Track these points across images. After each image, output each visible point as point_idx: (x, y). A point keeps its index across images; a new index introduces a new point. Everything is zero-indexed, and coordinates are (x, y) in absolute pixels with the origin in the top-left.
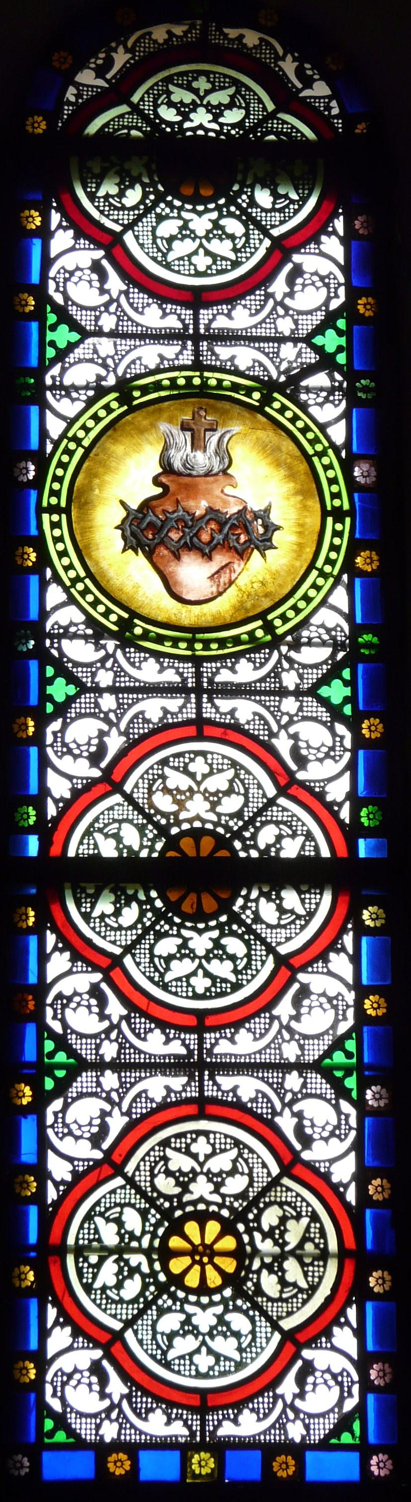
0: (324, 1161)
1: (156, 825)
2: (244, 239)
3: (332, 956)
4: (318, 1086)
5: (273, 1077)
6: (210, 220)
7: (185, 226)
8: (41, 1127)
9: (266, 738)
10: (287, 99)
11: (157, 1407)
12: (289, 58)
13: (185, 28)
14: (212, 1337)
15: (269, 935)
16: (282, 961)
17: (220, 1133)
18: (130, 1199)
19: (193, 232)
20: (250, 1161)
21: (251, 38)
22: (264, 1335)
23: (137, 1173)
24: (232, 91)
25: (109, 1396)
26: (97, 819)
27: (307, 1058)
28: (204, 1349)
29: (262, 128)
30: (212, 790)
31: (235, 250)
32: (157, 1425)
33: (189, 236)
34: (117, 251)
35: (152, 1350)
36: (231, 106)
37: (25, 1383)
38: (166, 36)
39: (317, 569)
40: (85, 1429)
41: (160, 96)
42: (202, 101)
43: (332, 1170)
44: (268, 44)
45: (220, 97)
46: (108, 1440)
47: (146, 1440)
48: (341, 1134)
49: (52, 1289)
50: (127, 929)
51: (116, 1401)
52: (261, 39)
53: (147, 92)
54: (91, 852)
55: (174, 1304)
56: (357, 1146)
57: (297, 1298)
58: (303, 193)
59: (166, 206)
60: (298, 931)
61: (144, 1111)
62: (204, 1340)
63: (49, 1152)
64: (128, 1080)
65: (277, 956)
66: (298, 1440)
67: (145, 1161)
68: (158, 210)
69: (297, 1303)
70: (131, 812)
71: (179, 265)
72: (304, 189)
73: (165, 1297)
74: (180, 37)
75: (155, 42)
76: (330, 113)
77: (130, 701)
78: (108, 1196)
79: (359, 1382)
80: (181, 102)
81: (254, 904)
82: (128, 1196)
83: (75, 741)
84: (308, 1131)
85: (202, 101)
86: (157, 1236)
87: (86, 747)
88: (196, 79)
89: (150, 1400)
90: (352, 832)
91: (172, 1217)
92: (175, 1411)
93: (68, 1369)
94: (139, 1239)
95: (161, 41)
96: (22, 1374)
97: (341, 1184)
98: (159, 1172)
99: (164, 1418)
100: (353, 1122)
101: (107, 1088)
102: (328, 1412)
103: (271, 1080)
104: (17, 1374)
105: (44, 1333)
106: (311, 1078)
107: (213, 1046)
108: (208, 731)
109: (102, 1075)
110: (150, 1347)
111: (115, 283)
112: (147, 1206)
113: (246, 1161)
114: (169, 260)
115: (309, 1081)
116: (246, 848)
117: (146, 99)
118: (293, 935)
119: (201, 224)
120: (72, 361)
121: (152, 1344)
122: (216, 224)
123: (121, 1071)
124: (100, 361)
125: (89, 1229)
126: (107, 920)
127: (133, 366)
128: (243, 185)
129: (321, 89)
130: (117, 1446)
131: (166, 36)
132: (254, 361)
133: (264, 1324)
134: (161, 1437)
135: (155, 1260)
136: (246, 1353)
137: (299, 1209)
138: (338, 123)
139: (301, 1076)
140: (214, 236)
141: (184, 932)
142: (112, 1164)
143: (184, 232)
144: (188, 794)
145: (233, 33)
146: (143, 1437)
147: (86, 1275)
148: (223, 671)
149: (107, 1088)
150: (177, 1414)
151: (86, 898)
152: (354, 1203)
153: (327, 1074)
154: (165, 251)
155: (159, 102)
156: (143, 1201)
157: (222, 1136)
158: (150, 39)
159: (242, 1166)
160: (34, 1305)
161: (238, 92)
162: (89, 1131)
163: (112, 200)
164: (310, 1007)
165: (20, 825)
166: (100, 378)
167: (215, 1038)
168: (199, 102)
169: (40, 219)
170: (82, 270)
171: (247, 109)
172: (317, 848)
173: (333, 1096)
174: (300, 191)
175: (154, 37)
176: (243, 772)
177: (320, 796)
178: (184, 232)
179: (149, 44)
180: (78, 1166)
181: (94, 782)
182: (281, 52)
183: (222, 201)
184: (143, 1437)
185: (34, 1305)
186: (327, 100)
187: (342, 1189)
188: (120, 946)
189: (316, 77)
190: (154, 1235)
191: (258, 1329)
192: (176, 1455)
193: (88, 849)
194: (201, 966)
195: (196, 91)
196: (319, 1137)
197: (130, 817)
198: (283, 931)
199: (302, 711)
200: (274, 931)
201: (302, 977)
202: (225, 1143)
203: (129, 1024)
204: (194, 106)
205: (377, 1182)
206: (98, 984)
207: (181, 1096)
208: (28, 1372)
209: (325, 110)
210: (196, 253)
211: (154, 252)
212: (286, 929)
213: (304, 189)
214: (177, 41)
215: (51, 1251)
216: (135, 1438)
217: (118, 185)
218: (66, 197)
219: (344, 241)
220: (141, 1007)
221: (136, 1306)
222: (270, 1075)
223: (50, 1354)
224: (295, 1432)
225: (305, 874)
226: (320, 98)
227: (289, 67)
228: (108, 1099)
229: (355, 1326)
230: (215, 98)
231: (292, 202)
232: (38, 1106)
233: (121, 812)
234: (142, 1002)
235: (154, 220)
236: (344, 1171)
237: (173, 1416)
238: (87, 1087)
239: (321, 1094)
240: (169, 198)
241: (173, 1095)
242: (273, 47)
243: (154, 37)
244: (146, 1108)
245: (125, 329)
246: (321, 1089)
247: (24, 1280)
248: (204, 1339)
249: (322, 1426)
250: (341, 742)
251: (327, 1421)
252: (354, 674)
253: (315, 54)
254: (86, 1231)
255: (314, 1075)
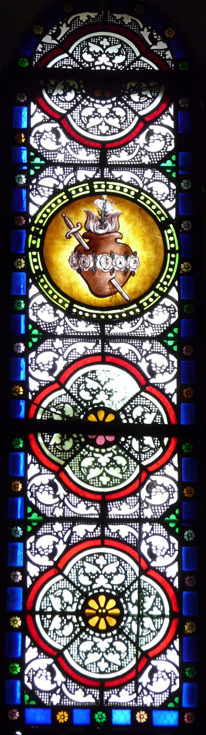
0: (162, 384)
1: (81, 591)
2: (125, 118)
3: (168, 651)
4: (159, 348)
5: (137, 343)
6: (108, 108)
7: (96, 111)
8: (25, 550)
9: (135, 362)
10: (146, 51)
11: (80, 688)
12: (146, 29)
13: (96, 14)
14: (107, 653)
15: (134, 107)
16: (143, 469)
17: (110, 554)
18: (68, 400)
19: (99, 114)
20: (125, 567)
21: (127, 20)
22: (133, 466)
23: (70, 574)
24: (119, 46)
25: (56, 682)
26: (50, 588)
27: (156, 704)
28: (103, 660)
29: (133, 65)
30: (108, 572)
31: (120, 123)
32: (79, 697)
33: (97, 116)
34: (60, 660)
35: (79, 475)
36: (119, 54)
37: (16, 627)
38: (87, 18)
39: (160, 283)
40: (44, 699)
41: (84, 48)
42: (104, 51)
43: (165, 387)
44: (136, 22)
45: (113, 50)
46: (55, 704)
47: (74, 704)
48: (169, 371)
49: (28, 629)
50: (69, 102)
51: (59, 685)
52: (132, 20)
53: (78, 46)
54: (49, 417)
55: (89, 453)
56: (179, 559)
57: (150, 452)
58: (154, 95)
59: (86, 634)
60: (148, 105)
61: (75, 542)
62: (102, 388)
63: (30, 378)
64: (68, 171)
65: (139, 116)
66: (149, 705)
67: (73, 568)
68: (82, 453)
69: (149, 454)
70: (70, 399)
71: (92, 130)
72: (154, 93)
73: (84, 633)
74: (94, 18)
75: (81, 21)
76: (165, 57)
77: (70, 171)
78: (58, 398)
79: (179, 677)
80: (94, 52)
81: (130, 441)
82: (69, 62)
83: (41, 363)
84: (154, 369)
85: (104, 51)
86: (80, 604)
87: (45, 489)
88: (102, 40)
89: (76, 684)
90: (177, 408)
91: (87, 595)
92: (88, 690)
93: (38, 484)
94: (71, 606)
95: (84, 21)
96: (18, 306)
97: (169, 394)
98: (85, 52)
99: (83, 693)
100: (176, 547)
101: (56, 530)
102: (164, 692)
103: (136, 345)
104: (15, 349)
105: (27, 467)
106: (155, 344)
107: (108, 698)
108: (107, 542)
109: (55, 341)
110: (78, 474)
111: (60, 678)
112: (79, 66)
113: (123, 567)
114: (88, 127)
115: (154, 345)
116: (127, 418)
117: (77, 50)
118: (146, 107)
119: (104, 110)
120: (42, 176)
121: (79, 473)
122: (111, 111)
123: (63, 339)
124: (55, 350)
125: (46, 601)
126: (59, 97)
127: (72, 180)
128: (126, 439)
129: (162, 45)
130: (60, 708)
131: (87, 18)
132: (129, 533)
133: (132, 647)
134: (81, 703)
135: (81, 84)
136: (125, 474)
137: (150, 592)
138: (169, 63)
139: (150, 343)
140: (110, 652)
141: (95, 455)
142: (59, 383)
143: (95, 114)
144: (97, 391)
145: (118, 16)
146: (72, 703)
147: (46, 439)
148: (113, 696)
149: (56, 531)
150: (89, 692)
151: (50, 87)
152: (177, 587)
153: (166, 525)
154: (86, 123)
155: (83, 51)
156: (74, 402)
157: (111, 555)
158: (79, 20)
159: (121, 570)
160: (22, 456)
161: (122, 47)
162: (48, 552)
163: (61, 101)
164: (158, 678)
165: (15, 447)
166: (55, 186)
167: (109, 694)
168: (103, 52)
169: (20, 668)
170: (47, 132)
171: (126, 55)
172: (162, 419)
173: (166, 353)
174: (153, 94)
175: (81, 19)
176: (123, 562)
177: (162, 391)
178: (95, 114)
179: (78, 22)
180: (42, 569)
181: (51, 383)
182: (142, 26)
183: (114, 99)
184: (72, 703)
185: (22, 456)
186: (164, 51)
187: (170, 397)
188: (65, 109)
189: (159, 39)
190: (79, 603)
191: (128, 115)
192: (88, 711)
193: (47, 415)
194: (101, 570)
195: (102, 46)
196: (159, 372)
197: (70, 402)
198: (141, 105)
199: (153, 349)
200: (137, 105)
201: (154, 662)
202: (113, 559)
203: (66, 686)
204: (101, 53)
205: (185, 181)
206: (51, 665)
207: (92, 352)
208: (16, 669)
209: (163, 56)
210: (101, 124)
211: (80, 123)
212: (142, 104)
213: (154, 93)
214: (92, 20)
215: (28, 613)
216: (68, 703)
217: (63, 90)
218: (40, 100)
219: (179, 653)
220: (72, 489)
221: (70, 453)
222: (136, 342)
223: (30, 296)
224: (147, 701)
225: (155, 430)
226: (160, 50)
227: (145, 34)
228: (57, 536)
229: (178, 650)
230: (111, 50)
231: (149, 99)
232: (25, 355)
233: (65, 399)
234: (74, 488)
235: (79, 458)
236: (172, 571)
237: (87, 693)
238: (47, 530)
239: (160, 352)
240: (88, 97)
241: (88, 351)
242: (138, 24)
243: (81, 19)
244: (76, 540)
245: (65, 703)
246: (160, 349)
247: (14, 716)
248: (104, 469)
249: (160, 699)
250: (172, 364)
251: (163, 696)
252: (177, 158)
253: (159, 29)
254: (45, 602)
255: (157, 343)
